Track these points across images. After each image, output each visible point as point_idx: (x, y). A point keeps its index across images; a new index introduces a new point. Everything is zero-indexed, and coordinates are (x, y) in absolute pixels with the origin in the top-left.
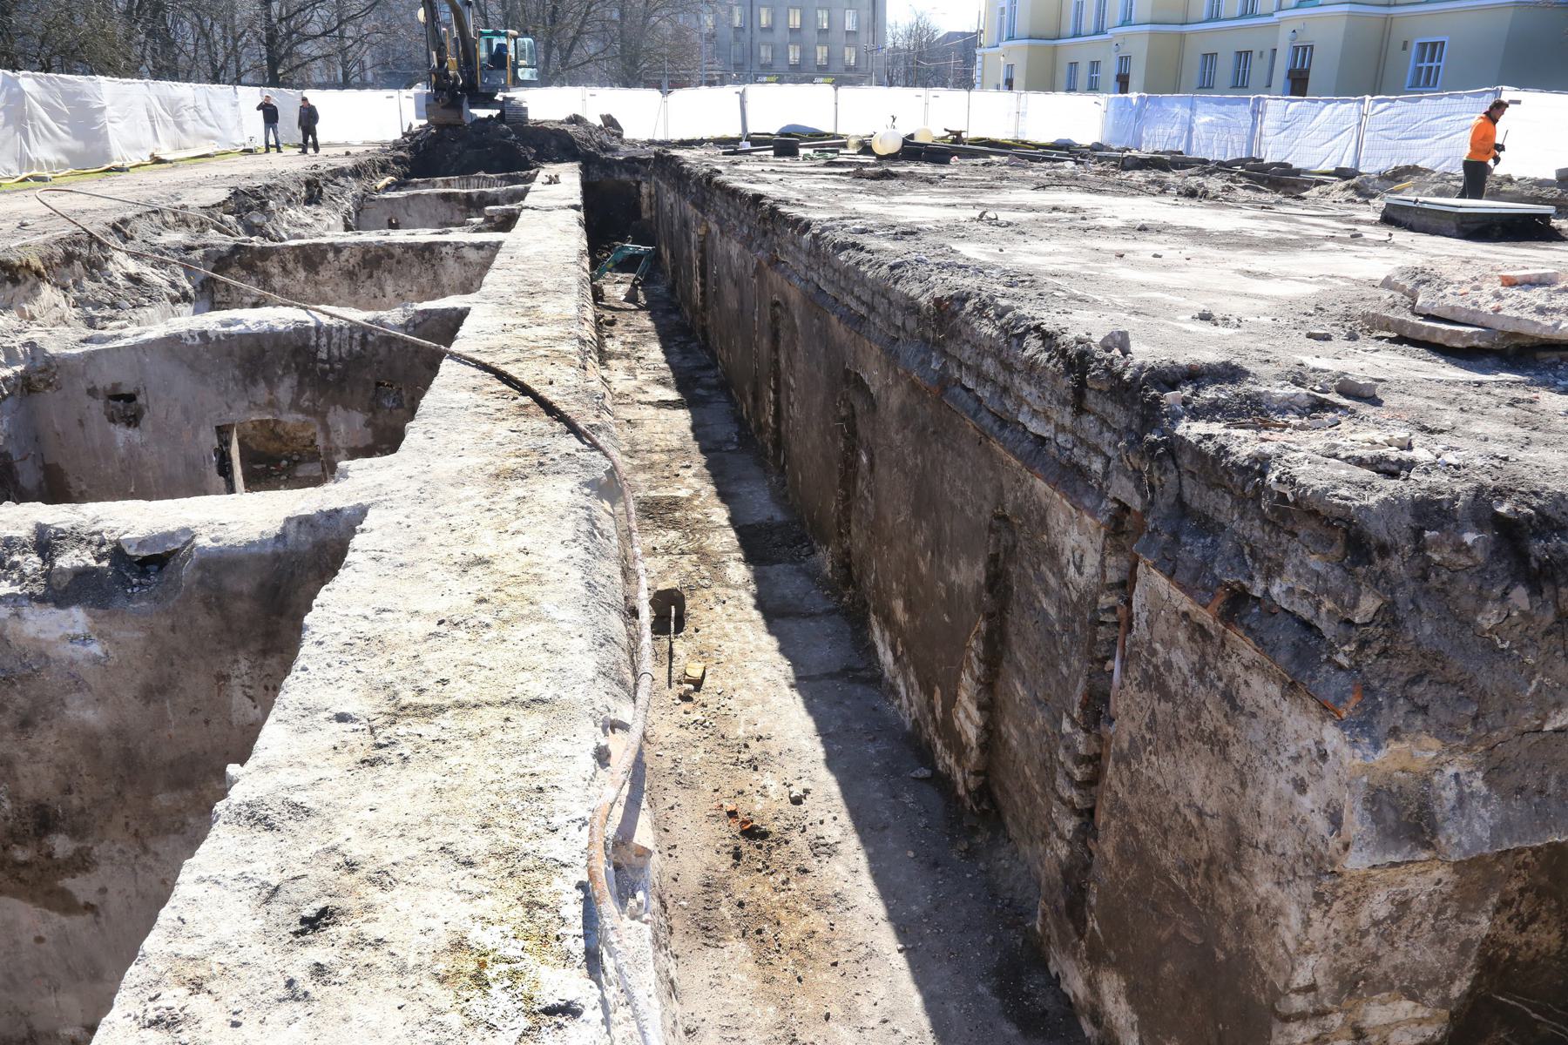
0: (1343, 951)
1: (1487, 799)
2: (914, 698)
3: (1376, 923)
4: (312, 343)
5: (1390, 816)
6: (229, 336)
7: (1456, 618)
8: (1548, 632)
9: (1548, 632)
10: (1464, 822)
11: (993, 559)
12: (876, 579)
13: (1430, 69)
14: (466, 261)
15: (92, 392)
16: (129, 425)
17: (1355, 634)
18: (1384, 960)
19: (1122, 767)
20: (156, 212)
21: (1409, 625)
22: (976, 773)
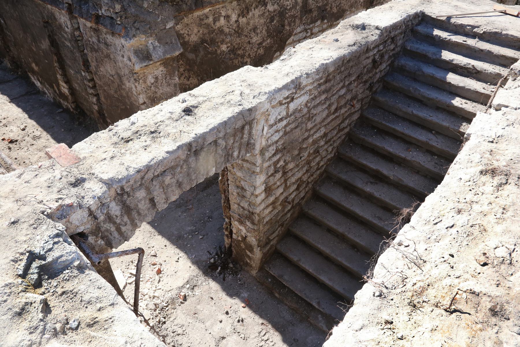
1: (160, 47)
2: (50, 92)
3: (152, 84)
5: (141, 55)
7: (139, 6)
8: (159, 6)
9: (159, 6)
11: (49, 36)
12: (24, 61)
17: (118, 15)
18: (158, 92)
19: (96, 76)
21: (129, 10)
22: (73, 103)
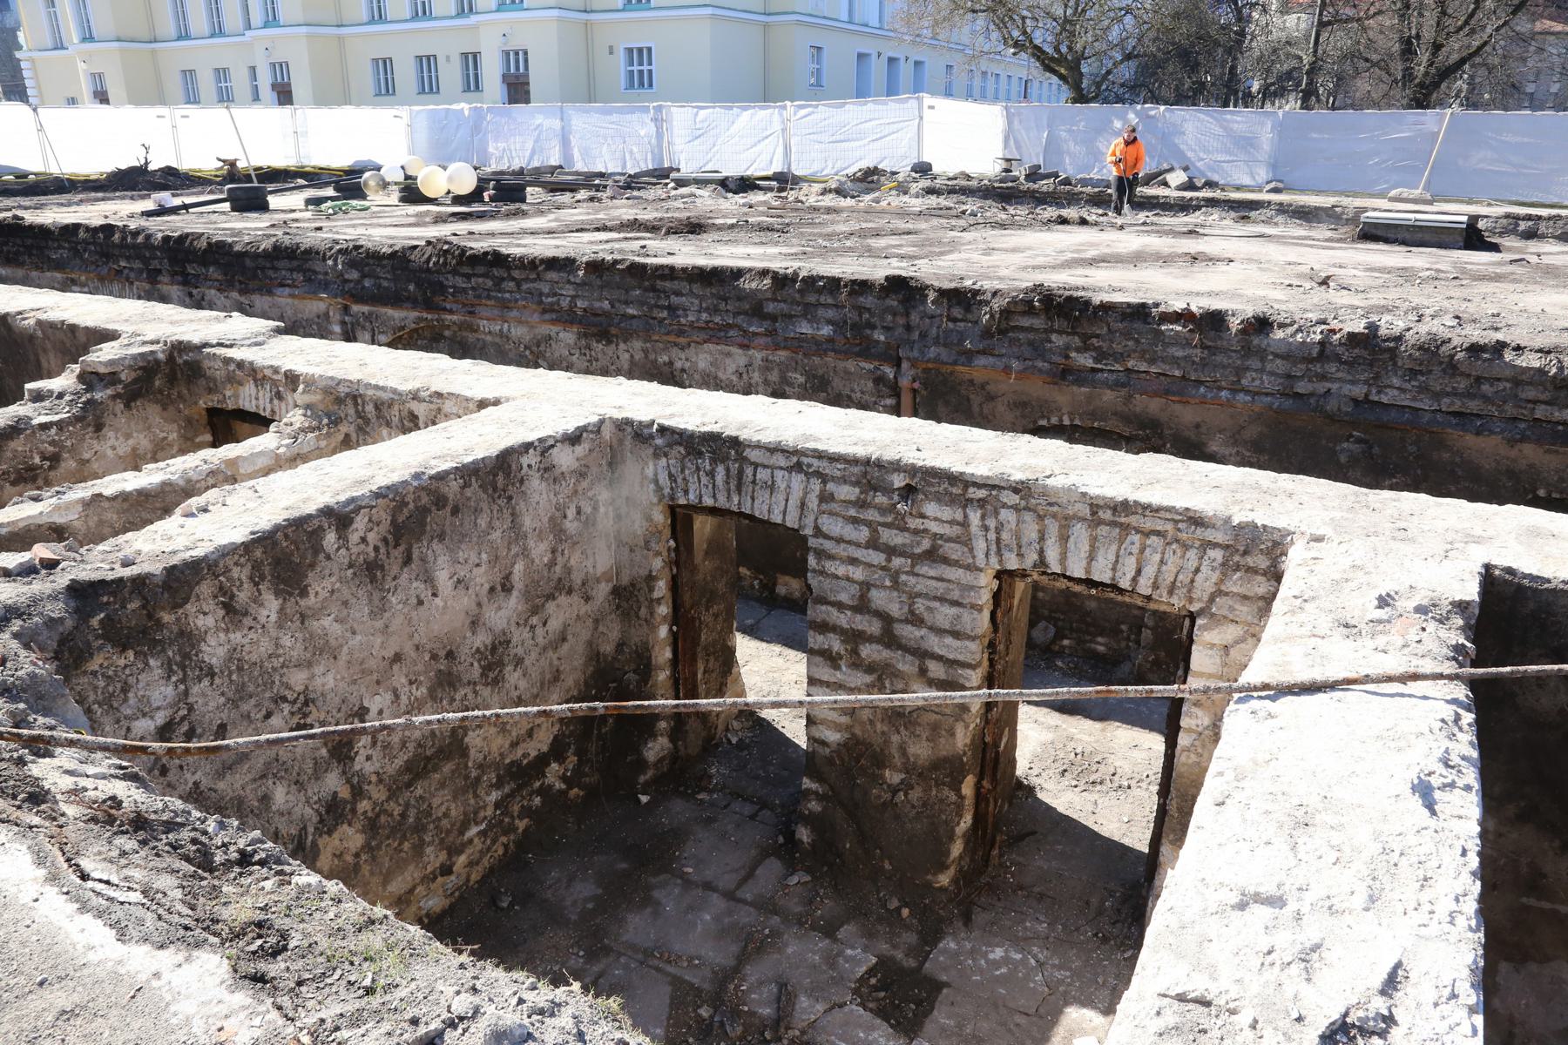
13: (641, 72)
14: (557, 472)
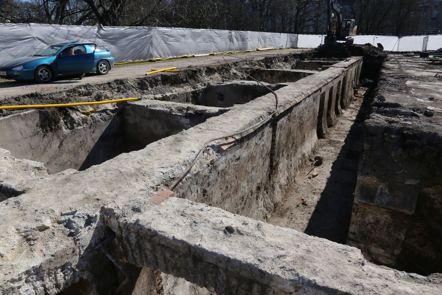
0: (361, 226)
3: (370, 223)
4: (256, 89)
6: (241, 85)
10: (380, 198)
15: (216, 93)
16: (221, 101)
20: (245, 61)
